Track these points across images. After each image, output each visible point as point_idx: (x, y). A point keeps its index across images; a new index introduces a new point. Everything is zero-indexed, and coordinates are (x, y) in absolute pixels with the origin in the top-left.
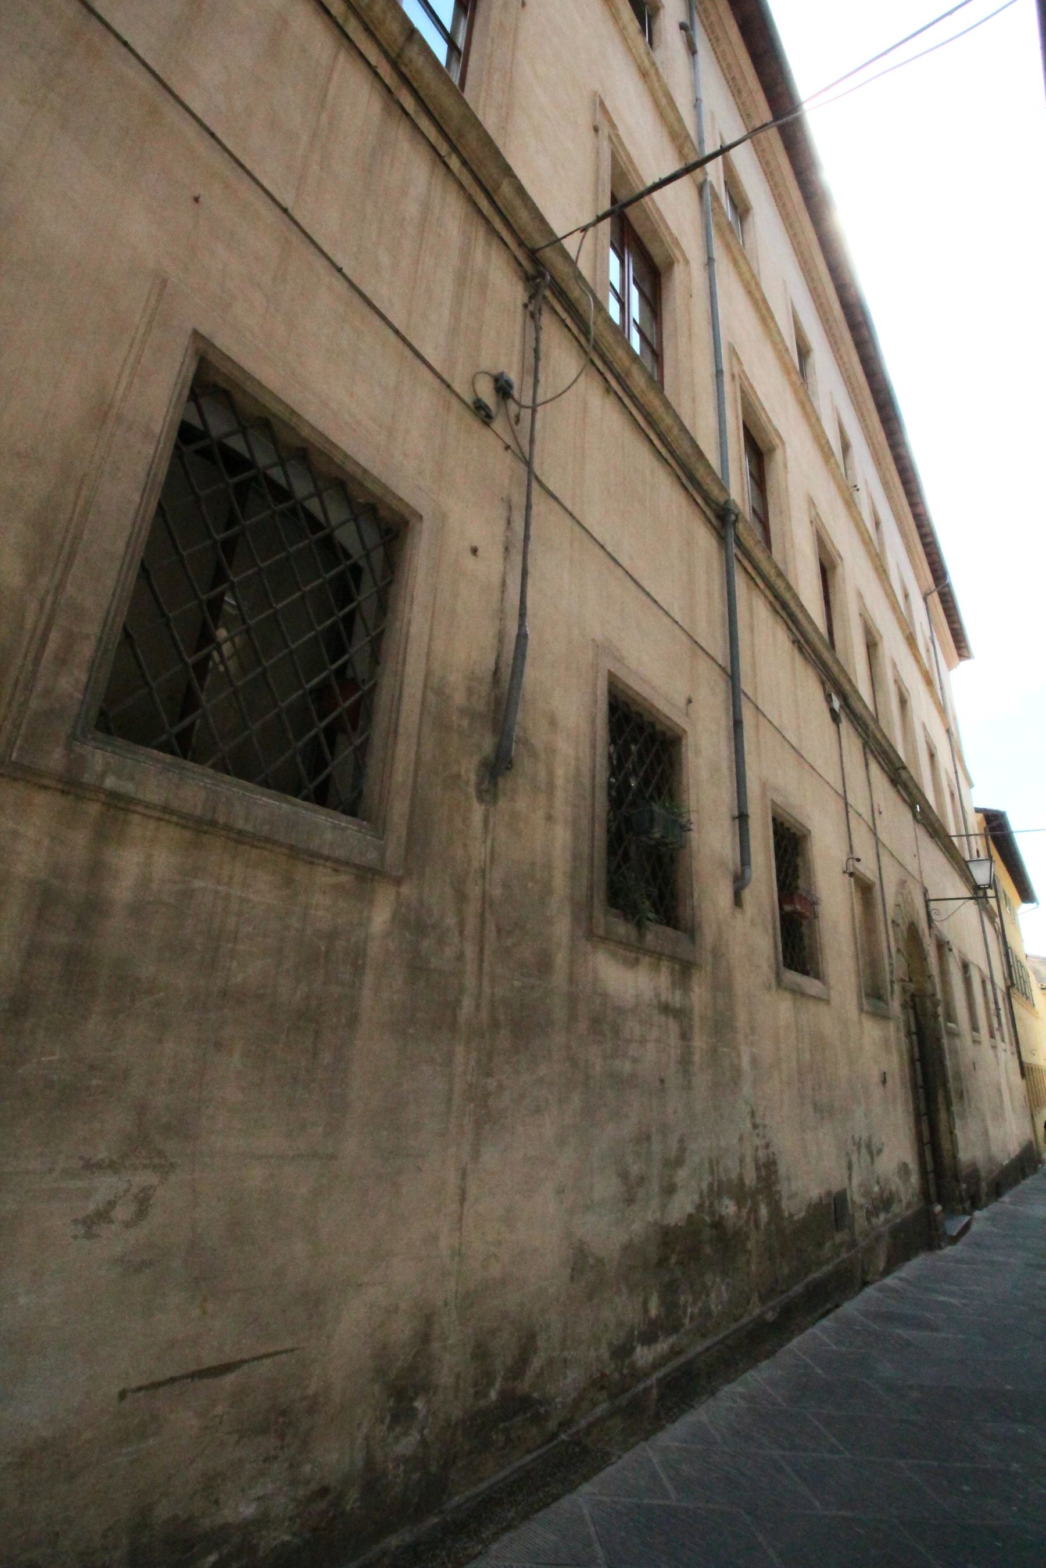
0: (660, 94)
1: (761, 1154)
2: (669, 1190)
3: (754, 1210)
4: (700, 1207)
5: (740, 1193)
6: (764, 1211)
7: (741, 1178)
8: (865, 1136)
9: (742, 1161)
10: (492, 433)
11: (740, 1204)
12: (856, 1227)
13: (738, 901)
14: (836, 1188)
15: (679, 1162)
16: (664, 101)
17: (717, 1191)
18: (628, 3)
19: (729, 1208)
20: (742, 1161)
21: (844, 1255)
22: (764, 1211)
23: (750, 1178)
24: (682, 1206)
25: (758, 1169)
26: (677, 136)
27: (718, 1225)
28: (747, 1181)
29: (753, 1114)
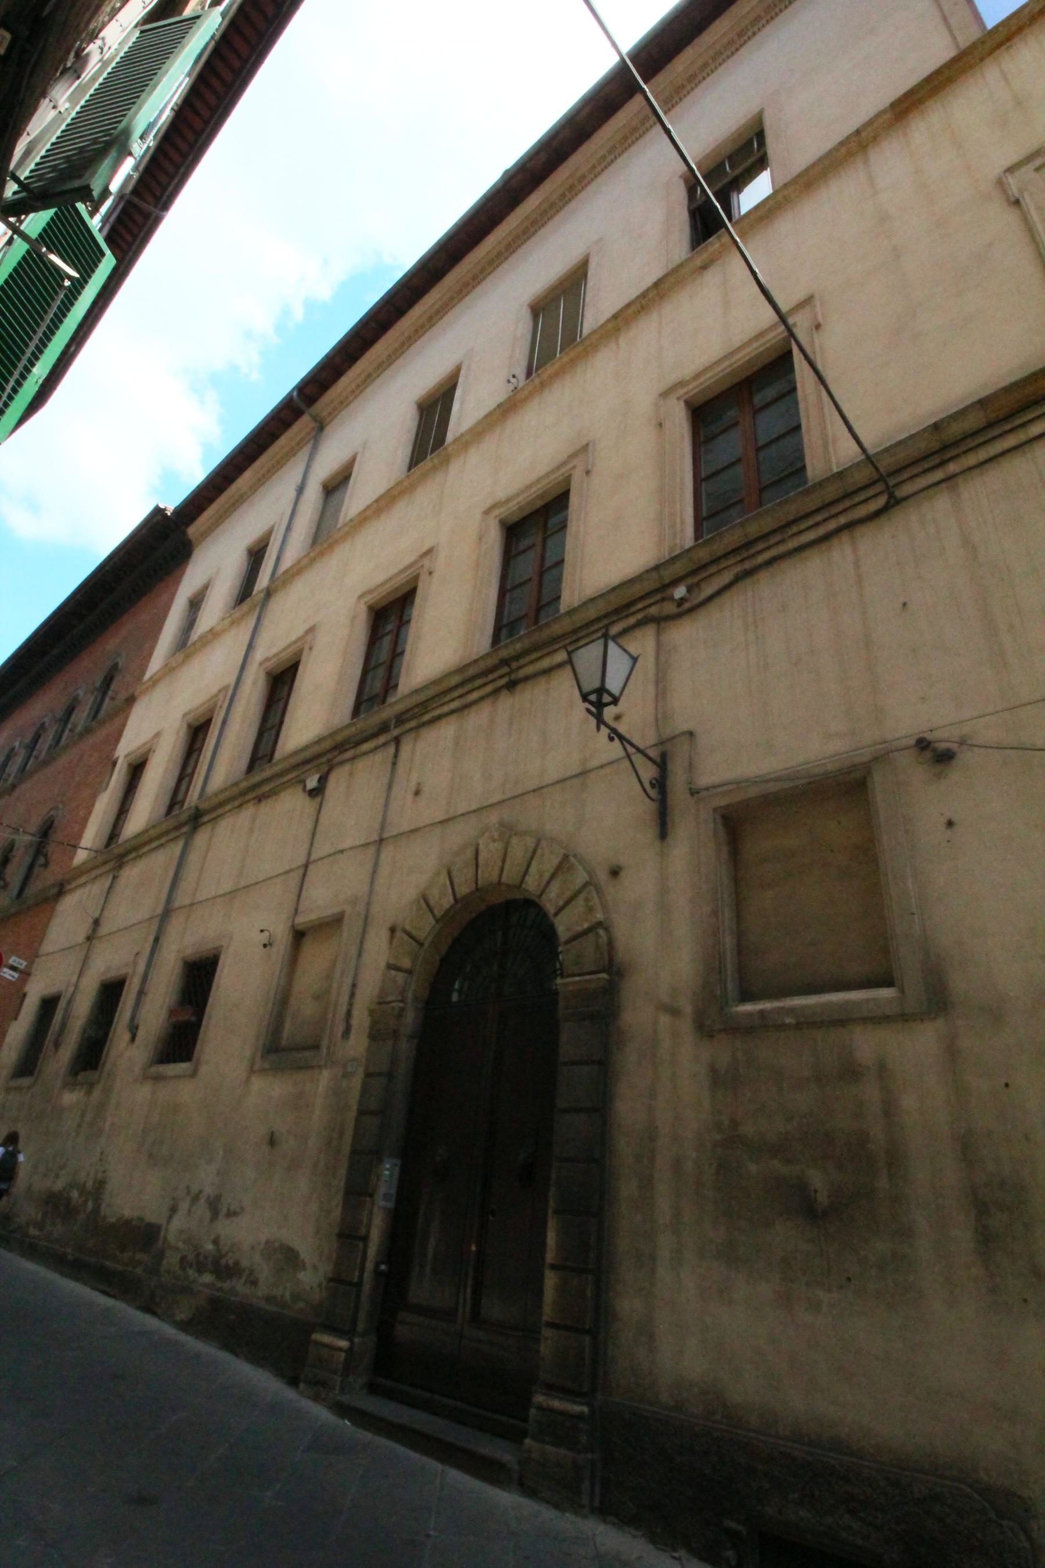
0: (272, 785)
1: (100, 1175)
2: (57, 1176)
3: (86, 1202)
4: (64, 1188)
5: (83, 1191)
6: (90, 1205)
7: (85, 1183)
8: (209, 1190)
9: (88, 1175)
10: (106, 913)
11: (81, 1196)
12: (165, 1262)
13: (133, 1039)
14: (151, 1217)
15: (62, 1167)
16: (266, 788)
17: (72, 1185)
18: (1041, 366)
19: (75, 1194)
20: (88, 1175)
21: (139, 1271)
22: (90, 1205)
23: (90, 1184)
24: (59, 1185)
25: (95, 1182)
26: (873, 483)
27: (69, 1199)
28: (87, 1185)
29: (102, 1153)
